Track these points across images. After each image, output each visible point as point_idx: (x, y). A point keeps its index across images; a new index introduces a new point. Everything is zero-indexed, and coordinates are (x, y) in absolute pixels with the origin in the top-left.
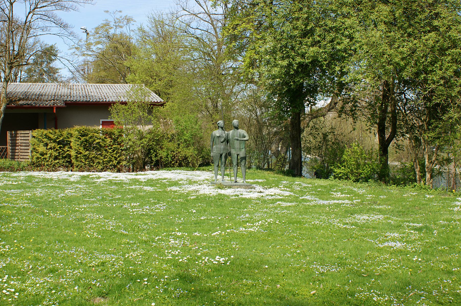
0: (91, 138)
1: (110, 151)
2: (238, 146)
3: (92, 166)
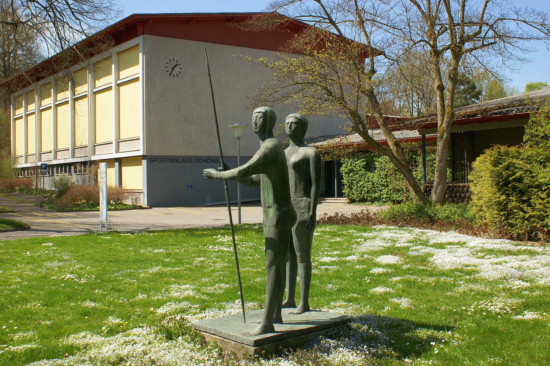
0: (507, 168)
1: (543, 195)
3: (512, 225)
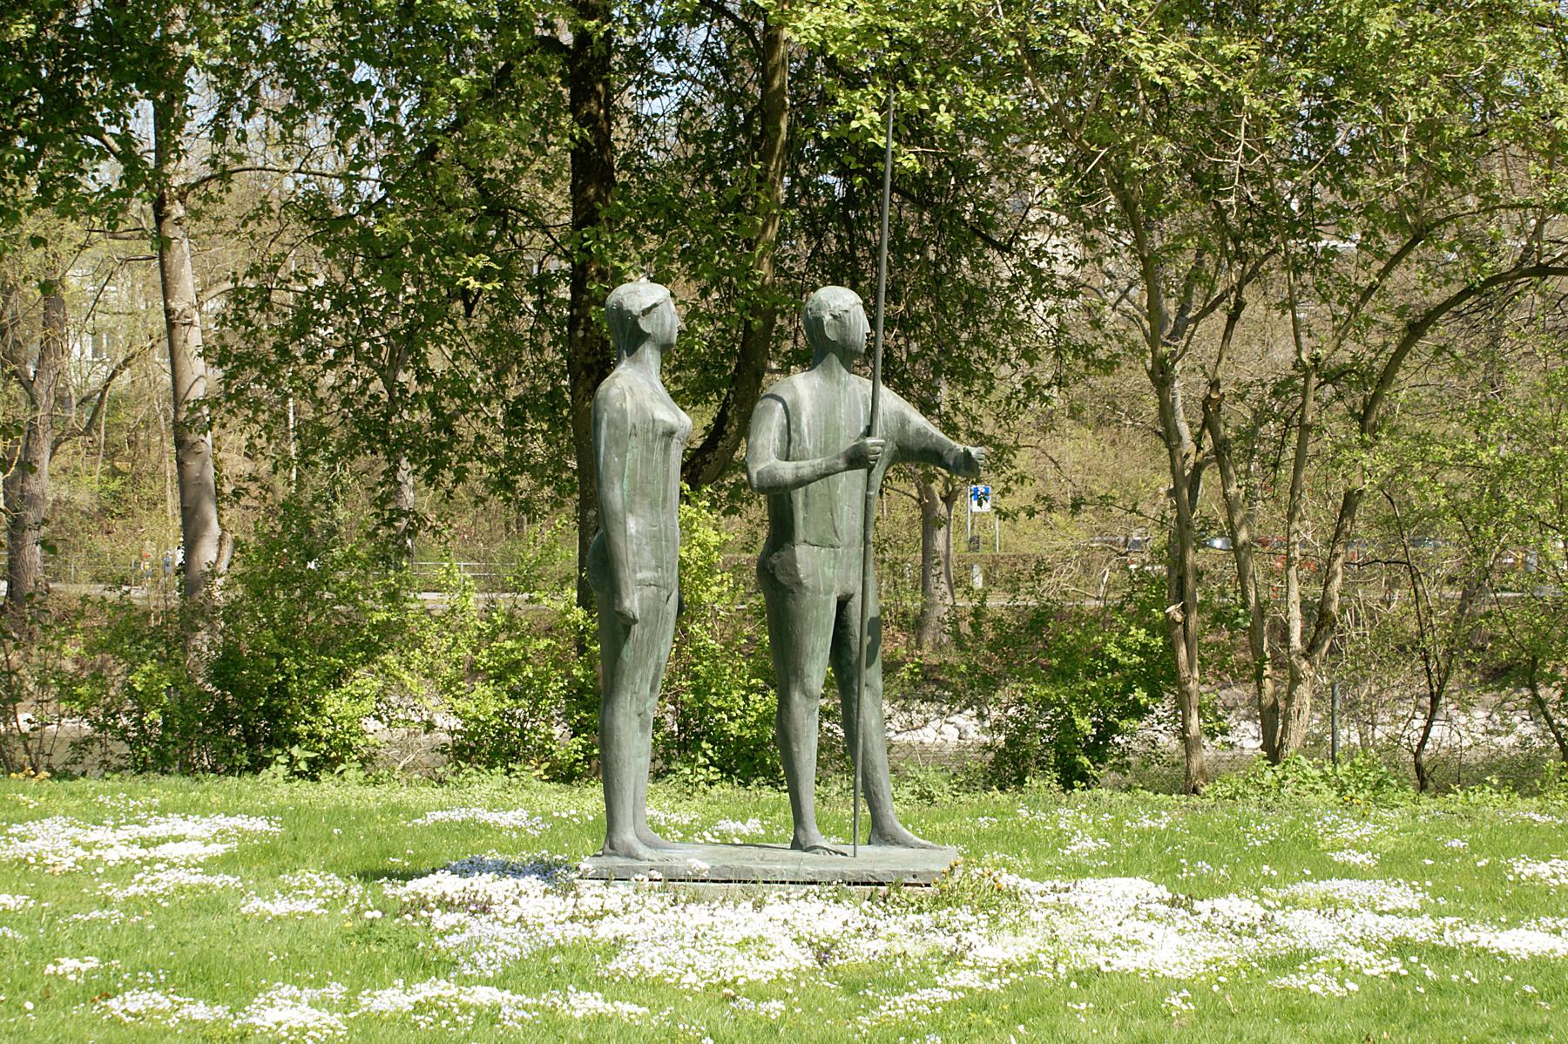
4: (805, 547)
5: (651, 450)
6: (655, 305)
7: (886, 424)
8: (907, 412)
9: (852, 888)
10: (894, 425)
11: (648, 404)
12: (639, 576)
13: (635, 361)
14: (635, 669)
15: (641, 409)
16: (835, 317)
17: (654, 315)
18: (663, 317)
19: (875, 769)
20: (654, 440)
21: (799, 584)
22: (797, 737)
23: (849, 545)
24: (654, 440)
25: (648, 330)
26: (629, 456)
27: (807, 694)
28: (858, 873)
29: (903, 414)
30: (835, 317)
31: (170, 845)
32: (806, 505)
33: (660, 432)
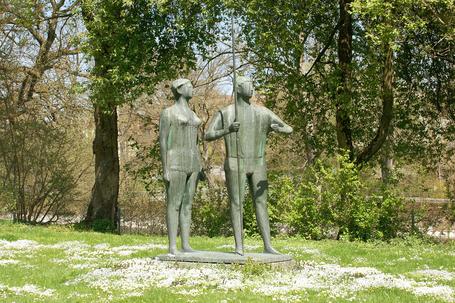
2: (253, 150)
4: (232, 158)
5: (177, 129)
6: (182, 85)
7: (263, 119)
8: (271, 115)
9: (226, 265)
10: (266, 119)
11: (177, 115)
12: (171, 167)
13: (179, 103)
14: (173, 196)
15: (173, 117)
16: (239, 86)
17: (182, 88)
18: (185, 89)
19: (263, 229)
20: (178, 126)
21: (230, 170)
22: (233, 218)
23: (249, 158)
24: (178, 126)
25: (181, 93)
26: (171, 131)
27: (236, 204)
28: (229, 260)
29: (269, 116)
30: (239, 86)
31: (215, 259)
32: (231, 145)
33: (180, 123)
